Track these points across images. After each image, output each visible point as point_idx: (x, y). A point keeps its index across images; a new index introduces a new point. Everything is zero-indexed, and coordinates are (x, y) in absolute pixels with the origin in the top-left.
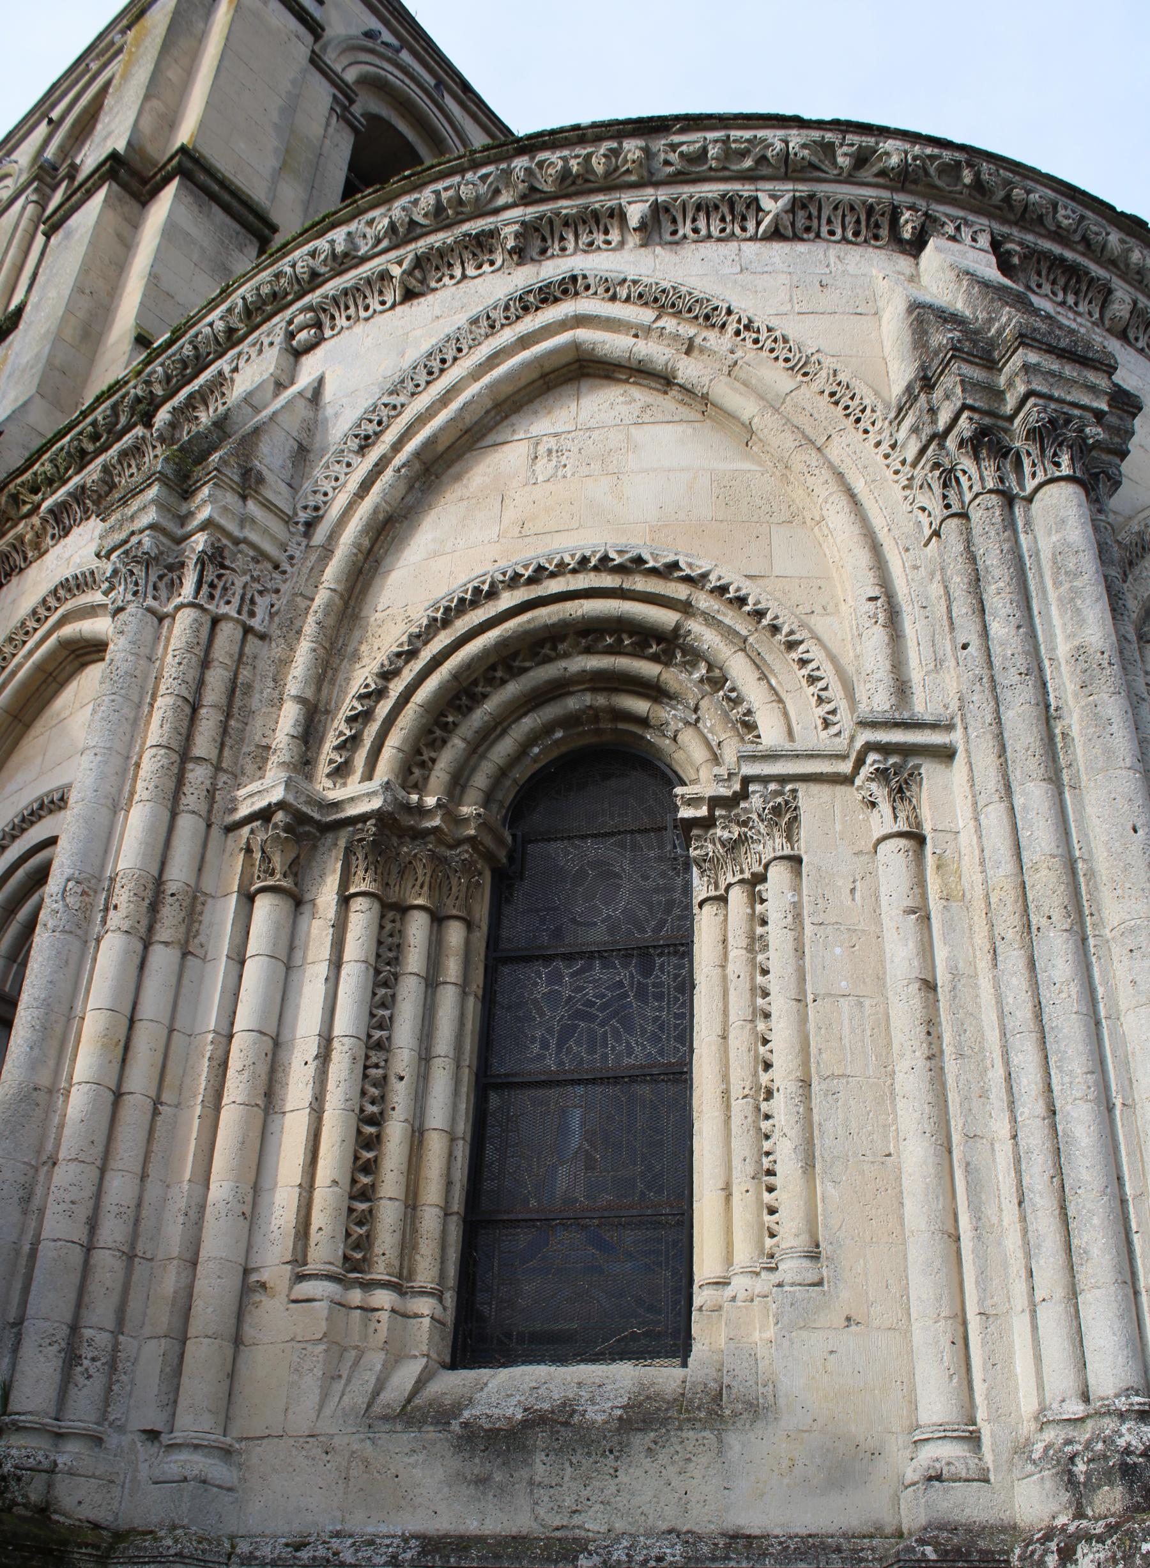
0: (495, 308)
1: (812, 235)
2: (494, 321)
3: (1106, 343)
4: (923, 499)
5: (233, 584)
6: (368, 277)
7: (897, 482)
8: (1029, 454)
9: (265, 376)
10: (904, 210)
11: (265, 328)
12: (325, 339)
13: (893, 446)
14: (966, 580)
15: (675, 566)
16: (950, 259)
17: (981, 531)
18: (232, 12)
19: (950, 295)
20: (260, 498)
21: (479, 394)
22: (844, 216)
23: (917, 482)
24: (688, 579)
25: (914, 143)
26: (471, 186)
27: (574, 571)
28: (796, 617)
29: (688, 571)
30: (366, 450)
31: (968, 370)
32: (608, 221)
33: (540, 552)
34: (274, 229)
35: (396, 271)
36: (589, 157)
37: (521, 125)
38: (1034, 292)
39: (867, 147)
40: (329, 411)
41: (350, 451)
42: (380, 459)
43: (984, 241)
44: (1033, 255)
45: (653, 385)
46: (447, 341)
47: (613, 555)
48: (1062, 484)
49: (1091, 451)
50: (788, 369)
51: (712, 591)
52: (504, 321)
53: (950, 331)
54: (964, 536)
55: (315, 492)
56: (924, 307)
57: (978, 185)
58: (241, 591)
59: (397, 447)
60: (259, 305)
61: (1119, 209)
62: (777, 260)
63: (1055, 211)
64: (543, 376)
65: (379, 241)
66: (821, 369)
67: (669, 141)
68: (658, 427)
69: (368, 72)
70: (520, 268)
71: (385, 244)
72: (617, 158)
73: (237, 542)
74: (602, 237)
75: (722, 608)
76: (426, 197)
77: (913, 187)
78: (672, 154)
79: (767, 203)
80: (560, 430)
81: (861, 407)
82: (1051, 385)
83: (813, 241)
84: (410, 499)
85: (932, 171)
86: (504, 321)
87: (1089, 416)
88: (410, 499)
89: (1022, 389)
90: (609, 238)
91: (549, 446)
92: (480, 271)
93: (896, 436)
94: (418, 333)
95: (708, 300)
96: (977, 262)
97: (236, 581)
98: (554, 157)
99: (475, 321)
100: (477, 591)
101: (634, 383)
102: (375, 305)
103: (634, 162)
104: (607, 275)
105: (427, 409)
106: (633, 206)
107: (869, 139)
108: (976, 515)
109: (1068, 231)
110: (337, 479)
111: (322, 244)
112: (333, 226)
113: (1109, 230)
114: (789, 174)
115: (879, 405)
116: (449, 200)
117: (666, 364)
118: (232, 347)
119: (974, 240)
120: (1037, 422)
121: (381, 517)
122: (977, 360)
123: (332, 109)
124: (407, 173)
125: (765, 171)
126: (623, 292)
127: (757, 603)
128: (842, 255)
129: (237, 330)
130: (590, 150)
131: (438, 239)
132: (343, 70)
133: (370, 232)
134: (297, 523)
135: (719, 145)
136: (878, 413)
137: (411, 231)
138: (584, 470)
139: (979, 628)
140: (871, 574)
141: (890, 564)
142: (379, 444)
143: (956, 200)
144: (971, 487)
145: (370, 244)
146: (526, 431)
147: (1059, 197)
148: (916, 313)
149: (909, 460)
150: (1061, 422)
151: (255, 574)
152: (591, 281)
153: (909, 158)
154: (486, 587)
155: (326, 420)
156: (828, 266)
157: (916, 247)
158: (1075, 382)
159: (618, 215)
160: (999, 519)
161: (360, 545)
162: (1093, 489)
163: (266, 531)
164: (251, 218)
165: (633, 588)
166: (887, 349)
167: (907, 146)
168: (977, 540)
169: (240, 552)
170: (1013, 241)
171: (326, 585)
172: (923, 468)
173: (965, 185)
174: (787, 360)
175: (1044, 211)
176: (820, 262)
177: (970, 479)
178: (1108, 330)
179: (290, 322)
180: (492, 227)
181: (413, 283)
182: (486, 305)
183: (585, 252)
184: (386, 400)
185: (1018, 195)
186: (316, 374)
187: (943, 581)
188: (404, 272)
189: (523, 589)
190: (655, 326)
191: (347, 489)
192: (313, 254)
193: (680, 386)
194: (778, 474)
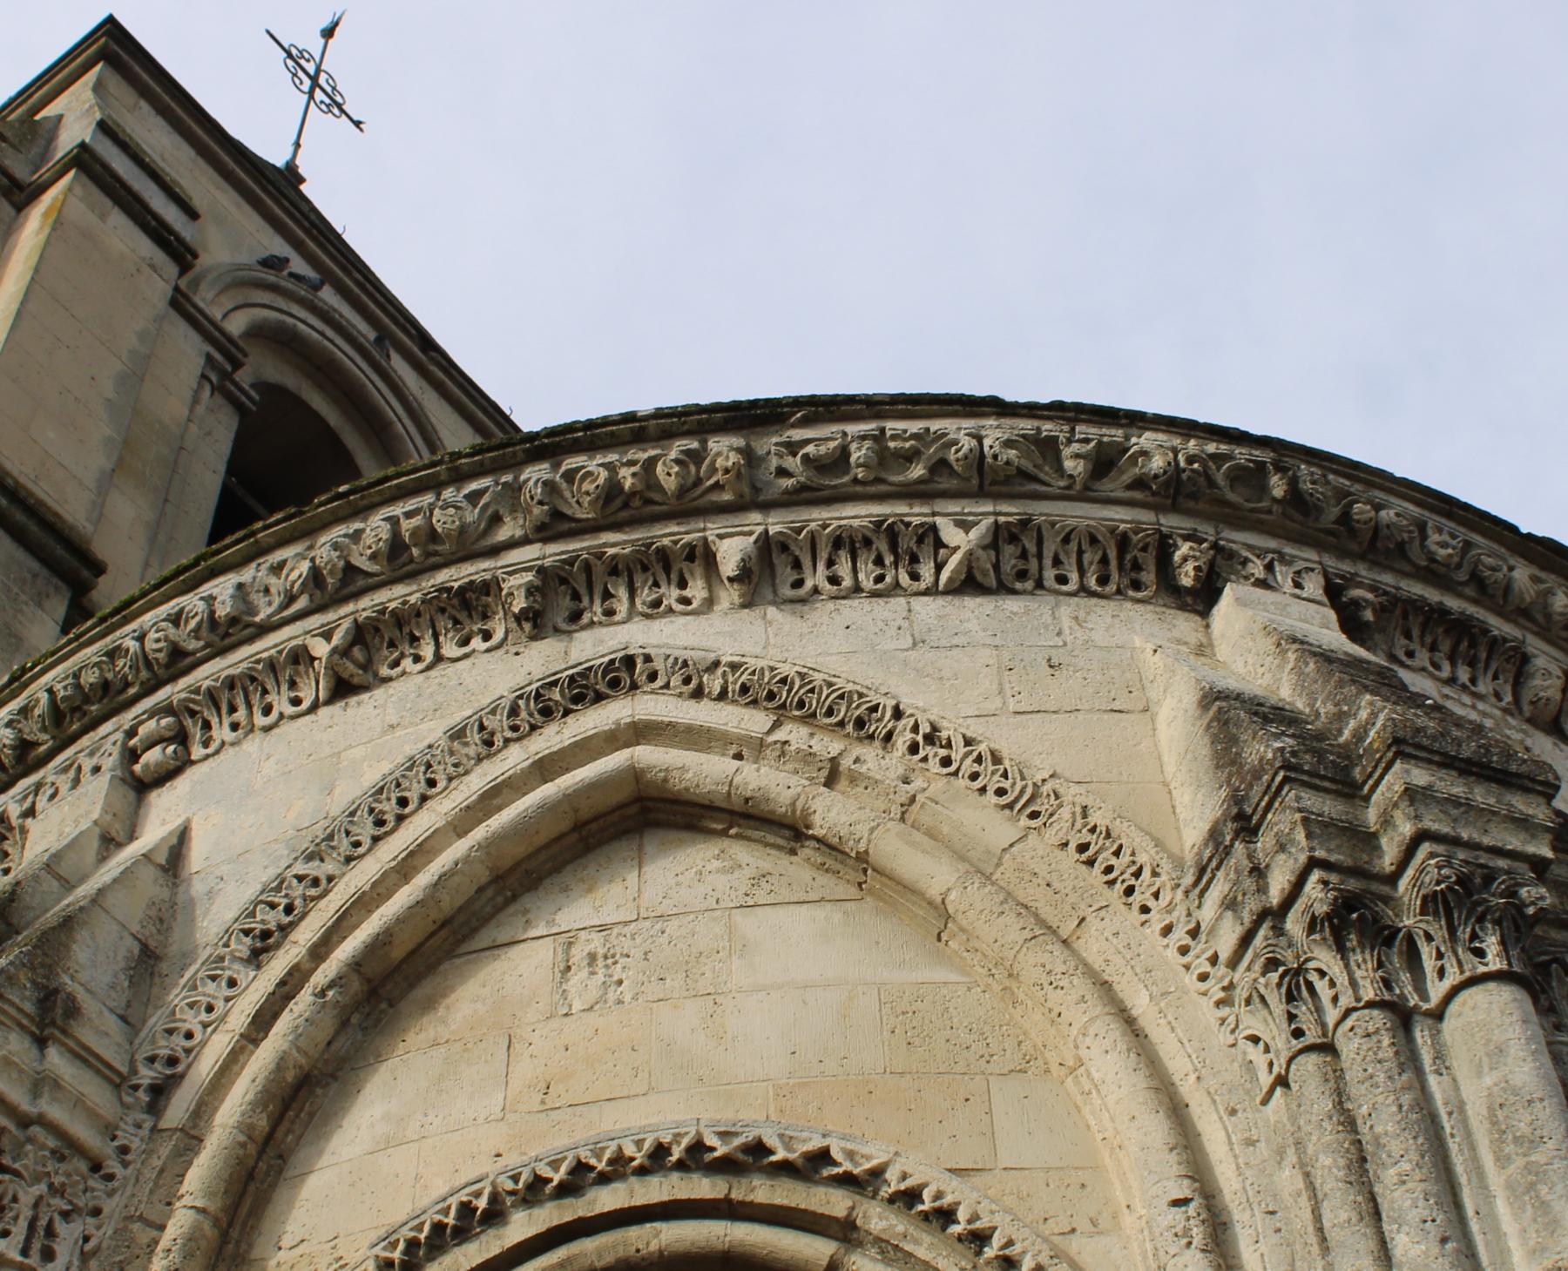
0: (493, 712)
1: (1029, 585)
2: (492, 734)
3: (1529, 742)
4: (1253, 1022)
5: (15, 1199)
6: (271, 658)
7: (1205, 994)
8: (1429, 938)
9: (84, 826)
10: (1180, 542)
11: (85, 741)
12: (193, 763)
13: (1194, 933)
14: (1342, 1162)
15: (822, 1157)
16: (1262, 617)
17: (1361, 1075)
18: (47, 230)
19: (1268, 676)
20: (71, 1044)
21: (467, 859)
22: (1080, 553)
23: (1241, 994)
24: (848, 1181)
25: (1187, 437)
26: (452, 511)
27: (642, 1171)
28: (1046, 1240)
29: (847, 1166)
30: (264, 957)
31: (1311, 800)
32: (685, 565)
33: (579, 1136)
34: (99, 569)
35: (321, 649)
36: (650, 464)
37: (530, 418)
38: (1402, 665)
39: (1110, 444)
40: (198, 888)
41: (235, 959)
42: (290, 973)
43: (1314, 586)
44: (1395, 608)
45: (771, 839)
46: (410, 769)
47: (711, 1140)
48: (1492, 985)
49: (1532, 927)
50: (1004, 807)
51: (891, 1200)
52: (509, 734)
53: (1277, 736)
54: (1332, 1084)
55: (170, 1032)
56: (1227, 698)
57: (1296, 498)
58: (30, 1213)
59: (319, 951)
60: (77, 703)
61: (1524, 530)
62: (972, 625)
63: (1424, 536)
64: (578, 827)
65: (291, 599)
66: (1060, 806)
67: (783, 439)
68: (781, 912)
69: (265, 320)
70: (535, 644)
71: (302, 603)
72: (698, 464)
73: (25, 1122)
74: (675, 593)
75: (911, 1230)
76: (376, 528)
77: (1191, 504)
78: (790, 459)
79: (951, 534)
80: (609, 920)
81: (1133, 869)
82: (1455, 820)
83: (1032, 593)
84: (342, 1044)
85: (1220, 478)
86: (509, 734)
87: (1522, 867)
88: (342, 1044)
89: (1406, 829)
90: (687, 593)
91: (591, 947)
92: (466, 650)
93: (1197, 914)
94: (357, 753)
95: (861, 695)
96: (1305, 621)
97: (21, 1195)
98: (594, 465)
99: (458, 734)
100: (466, 1209)
101: (738, 836)
102: (281, 704)
103: (727, 471)
104: (687, 654)
105: (374, 885)
106: (727, 542)
107: (1113, 432)
108: (1349, 1046)
109: (1447, 566)
110: (210, 1009)
111: (192, 602)
112: (213, 573)
113: (1512, 562)
114: (986, 488)
115: (1163, 863)
116: (415, 532)
117: (793, 804)
118: (25, 775)
119: (1298, 585)
120: (1438, 883)
121: (290, 1076)
122: (1327, 784)
123: (204, 376)
124: (342, 489)
125: (945, 483)
126: (714, 684)
127: (974, 1218)
128: (1082, 615)
129: (37, 744)
130: (652, 453)
131: (393, 596)
132: (225, 316)
133: (276, 584)
134: (136, 1088)
135: (867, 444)
136: (1164, 877)
137: (351, 582)
138: (654, 990)
139: (1372, 1244)
140: (1173, 1158)
141: (1205, 1138)
142: (287, 946)
143: (1262, 522)
144: (1335, 999)
145: (275, 605)
146: (551, 923)
147: (1427, 513)
148: (1214, 708)
149: (1224, 955)
150: (1478, 881)
151: (57, 1180)
152: (658, 664)
153: (1181, 458)
154: (482, 1203)
155: (191, 903)
156: (1059, 634)
157: (1203, 598)
158: (1494, 813)
159: (704, 556)
160: (1390, 1053)
161: (251, 1127)
162: (1544, 991)
163: (79, 1102)
164: (60, 551)
165: (748, 1199)
166: (1170, 769)
167: (1177, 441)
168: (1355, 1089)
169: (30, 1140)
170: (1360, 585)
171: (187, 1201)
172: (1249, 969)
173: (1274, 500)
174: (1001, 792)
175: (1405, 536)
176: (1046, 627)
177: (1332, 984)
178: (1529, 721)
179: (132, 733)
180: (488, 576)
181: (349, 669)
182: (477, 706)
183: (647, 616)
184: (300, 868)
185: (1362, 513)
186: (175, 823)
187: (1302, 1164)
188: (334, 651)
189: (550, 1205)
190: (771, 739)
191: (229, 1026)
192: (176, 619)
193: (818, 840)
194: (996, 987)
